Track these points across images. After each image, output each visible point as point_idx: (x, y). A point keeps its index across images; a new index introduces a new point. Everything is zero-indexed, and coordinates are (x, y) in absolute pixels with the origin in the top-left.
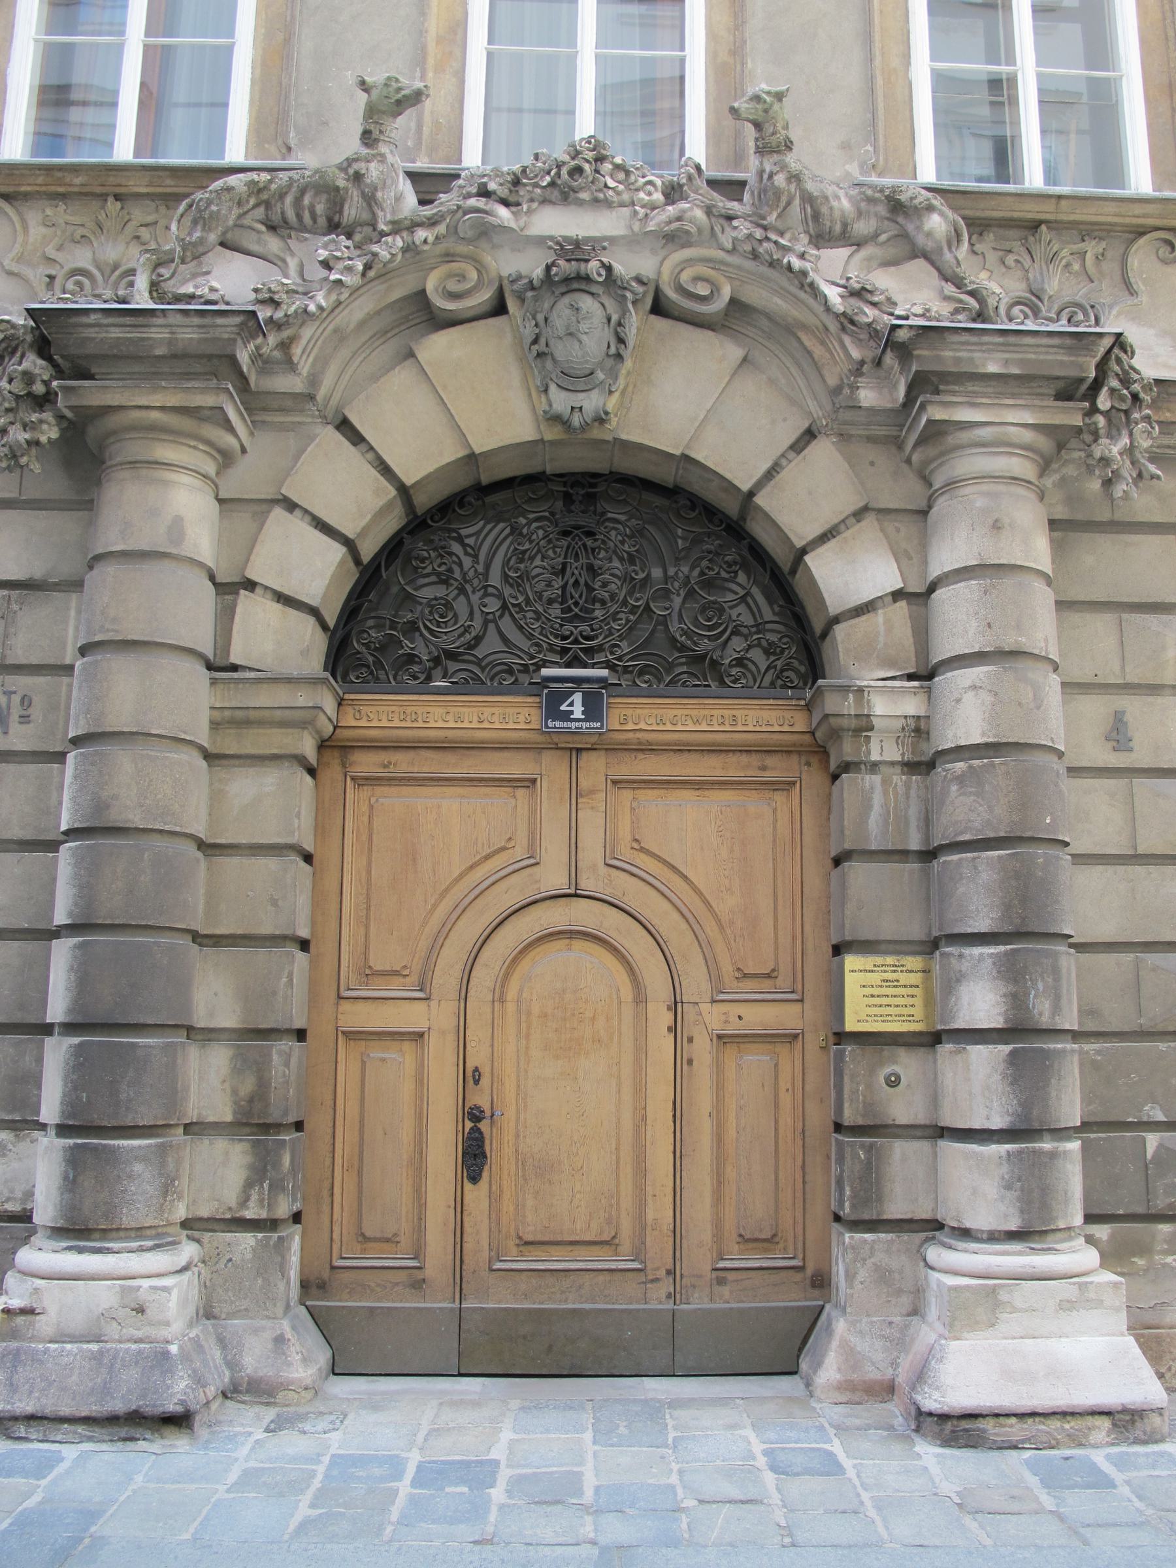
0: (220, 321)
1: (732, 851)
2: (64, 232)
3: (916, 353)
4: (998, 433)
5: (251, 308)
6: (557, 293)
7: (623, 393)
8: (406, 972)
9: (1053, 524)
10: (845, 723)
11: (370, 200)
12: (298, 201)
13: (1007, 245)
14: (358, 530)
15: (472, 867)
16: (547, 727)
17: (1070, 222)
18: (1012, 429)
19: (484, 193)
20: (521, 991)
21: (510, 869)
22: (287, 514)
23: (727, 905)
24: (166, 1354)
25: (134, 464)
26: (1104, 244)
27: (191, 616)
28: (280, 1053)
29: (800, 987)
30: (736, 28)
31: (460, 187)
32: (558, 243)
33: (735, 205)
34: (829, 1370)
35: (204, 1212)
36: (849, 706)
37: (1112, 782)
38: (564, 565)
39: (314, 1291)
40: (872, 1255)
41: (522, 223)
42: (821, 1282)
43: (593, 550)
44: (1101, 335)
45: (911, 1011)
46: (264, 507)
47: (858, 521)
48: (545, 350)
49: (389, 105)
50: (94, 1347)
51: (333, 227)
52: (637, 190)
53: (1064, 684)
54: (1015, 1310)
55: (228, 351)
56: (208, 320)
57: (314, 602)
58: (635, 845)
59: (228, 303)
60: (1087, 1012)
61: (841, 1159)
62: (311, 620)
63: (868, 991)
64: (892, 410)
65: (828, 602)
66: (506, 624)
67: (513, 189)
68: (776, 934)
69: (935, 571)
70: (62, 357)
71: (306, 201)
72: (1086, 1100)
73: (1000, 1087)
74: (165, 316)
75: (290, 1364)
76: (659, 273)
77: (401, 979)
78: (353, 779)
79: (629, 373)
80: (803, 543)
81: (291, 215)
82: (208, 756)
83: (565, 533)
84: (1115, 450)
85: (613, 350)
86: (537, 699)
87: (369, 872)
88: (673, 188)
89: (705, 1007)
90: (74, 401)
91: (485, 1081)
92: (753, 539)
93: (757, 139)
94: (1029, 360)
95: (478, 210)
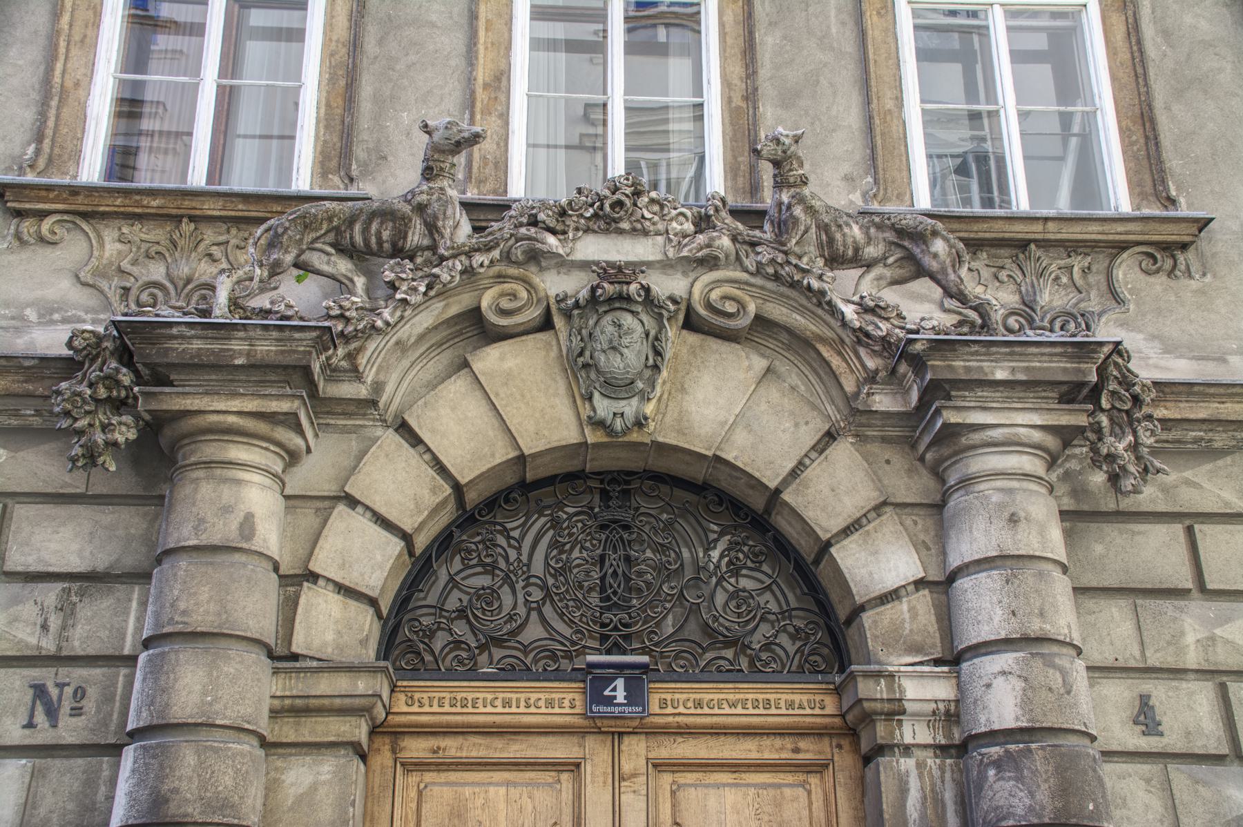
2: (139, 248)
4: (1009, 437)
7: (659, 400)
9: (1064, 514)
11: (432, 228)
12: (366, 230)
13: (1000, 263)
14: (416, 525)
16: (591, 711)
18: (1022, 430)
19: (534, 222)
22: (350, 511)
25: (209, 464)
27: (256, 610)
30: (748, 77)
33: (757, 233)
36: (880, 690)
37: (1146, 767)
38: (602, 559)
41: (568, 250)
43: (629, 542)
46: (327, 504)
47: (879, 516)
48: (591, 362)
52: (671, 220)
53: (1088, 668)
55: (304, 362)
62: (371, 611)
66: (548, 610)
69: (954, 561)
70: (145, 365)
71: (374, 227)
74: (245, 330)
78: (403, 764)
79: (664, 383)
81: (358, 239)
82: (264, 743)
83: (603, 527)
84: (1121, 446)
85: (651, 362)
86: (582, 685)
88: (701, 218)
90: (154, 406)
92: (777, 531)
93: (775, 176)
95: (530, 239)
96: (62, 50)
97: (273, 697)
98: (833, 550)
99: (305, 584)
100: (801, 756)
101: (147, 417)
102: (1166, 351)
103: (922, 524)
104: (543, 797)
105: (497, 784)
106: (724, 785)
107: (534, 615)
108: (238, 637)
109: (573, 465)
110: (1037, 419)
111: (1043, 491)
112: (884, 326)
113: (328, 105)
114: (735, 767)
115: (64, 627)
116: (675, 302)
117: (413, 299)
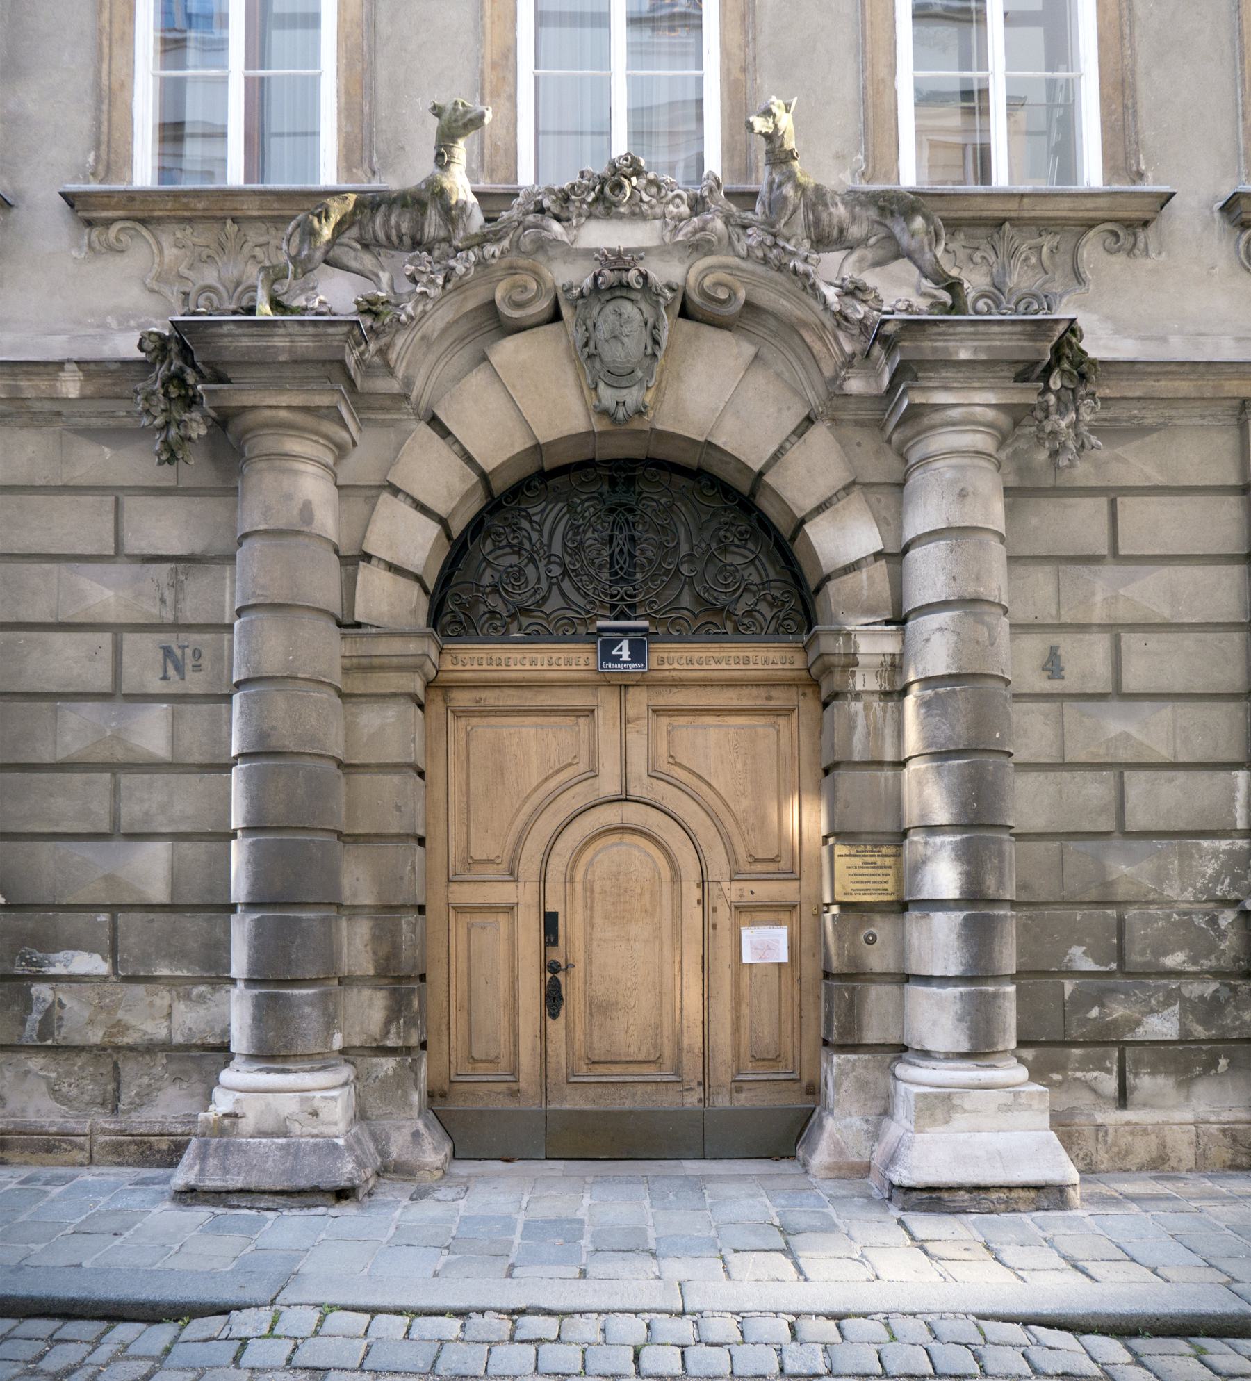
0: (331, 330)
1: (745, 764)
2: (193, 252)
4: (966, 413)
5: (355, 318)
6: (603, 300)
7: (658, 388)
9: (1007, 491)
10: (835, 660)
15: (546, 779)
17: (1030, 219)
18: (978, 409)
20: (586, 874)
21: (576, 780)
24: (335, 1146)
26: (1058, 237)
27: (323, 585)
28: (409, 923)
33: (750, 215)
34: (821, 1157)
35: (357, 1042)
36: (839, 646)
38: (611, 537)
40: (853, 1070)
42: (813, 1090)
43: (634, 524)
44: (1057, 321)
45: (886, 886)
46: (374, 492)
49: (454, 126)
50: (282, 1141)
51: (416, 244)
52: (668, 203)
53: (1011, 625)
54: (965, 1111)
55: (339, 357)
56: (321, 330)
57: (418, 571)
58: (671, 760)
60: (1022, 887)
61: (829, 999)
62: (417, 586)
63: (852, 871)
64: (876, 397)
65: (823, 562)
66: (566, 585)
67: (563, 204)
69: (909, 535)
72: (1020, 953)
73: (956, 944)
75: (424, 1152)
76: (686, 280)
80: (803, 514)
81: (381, 235)
82: (342, 695)
84: (1063, 424)
85: (649, 351)
87: (468, 784)
88: (697, 201)
89: (725, 885)
90: (217, 403)
94: (995, 347)
96: (106, 50)
97: (343, 657)
98: (806, 527)
100: (772, 703)
101: (213, 414)
102: (1117, 332)
107: (555, 588)
108: (309, 607)
109: (583, 454)
110: (992, 398)
111: (992, 467)
112: (862, 309)
113: (347, 93)
114: (719, 712)
115: (177, 601)
116: (672, 289)
117: (433, 292)
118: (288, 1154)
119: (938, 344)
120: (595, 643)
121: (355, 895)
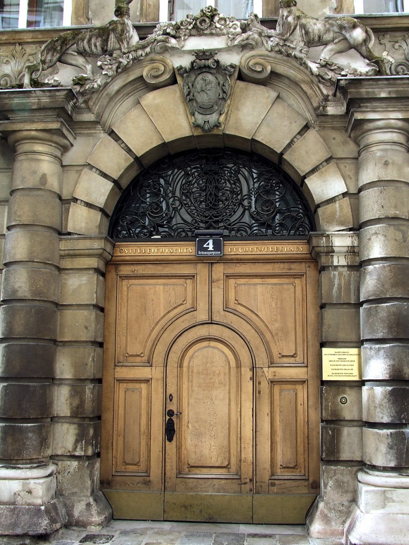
0: (57, 94)
1: (277, 304)
3: (349, 91)
8: (142, 355)
10: (322, 249)
13: (396, 40)
15: (169, 312)
16: (198, 254)
18: (393, 121)
20: (189, 363)
21: (184, 313)
23: (275, 326)
24: (40, 510)
25: (26, 153)
28: (89, 389)
29: (306, 361)
31: (156, 32)
32: (197, 53)
39: (105, 484)
40: (335, 475)
45: (351, 371)
46: (81, 168)
47: (328, 164)
52: (230, 28)
54: (394, 501)
56: (53, 93)
58: (236, 302)
59: (62, 86)
63: (332, 363)
65: (315, 198)
68: (296, 338)
69: (361, 184)
71: (93, 41)
77: (140, 358)
78: (120, 277)
83: (206, 174)
86: (194, 243)
89: (266, 370)
91: (175, 400)
99: (72, 203)
103: (348, 168)
104: (179, 290)
105: (160, 285)
106: (258, 284)
109: (192, 146)
110: (400, 115)
118: (14, 514)
119: (369, 90)
120: (195, 241)
121: (62, 374)
